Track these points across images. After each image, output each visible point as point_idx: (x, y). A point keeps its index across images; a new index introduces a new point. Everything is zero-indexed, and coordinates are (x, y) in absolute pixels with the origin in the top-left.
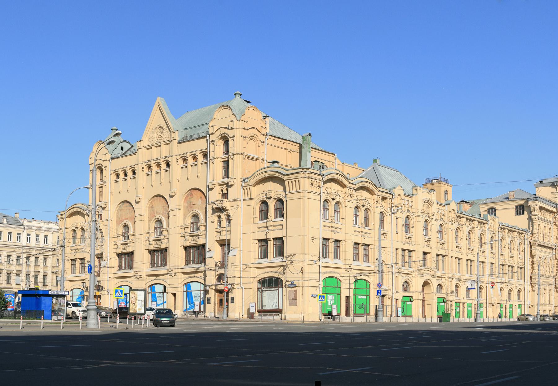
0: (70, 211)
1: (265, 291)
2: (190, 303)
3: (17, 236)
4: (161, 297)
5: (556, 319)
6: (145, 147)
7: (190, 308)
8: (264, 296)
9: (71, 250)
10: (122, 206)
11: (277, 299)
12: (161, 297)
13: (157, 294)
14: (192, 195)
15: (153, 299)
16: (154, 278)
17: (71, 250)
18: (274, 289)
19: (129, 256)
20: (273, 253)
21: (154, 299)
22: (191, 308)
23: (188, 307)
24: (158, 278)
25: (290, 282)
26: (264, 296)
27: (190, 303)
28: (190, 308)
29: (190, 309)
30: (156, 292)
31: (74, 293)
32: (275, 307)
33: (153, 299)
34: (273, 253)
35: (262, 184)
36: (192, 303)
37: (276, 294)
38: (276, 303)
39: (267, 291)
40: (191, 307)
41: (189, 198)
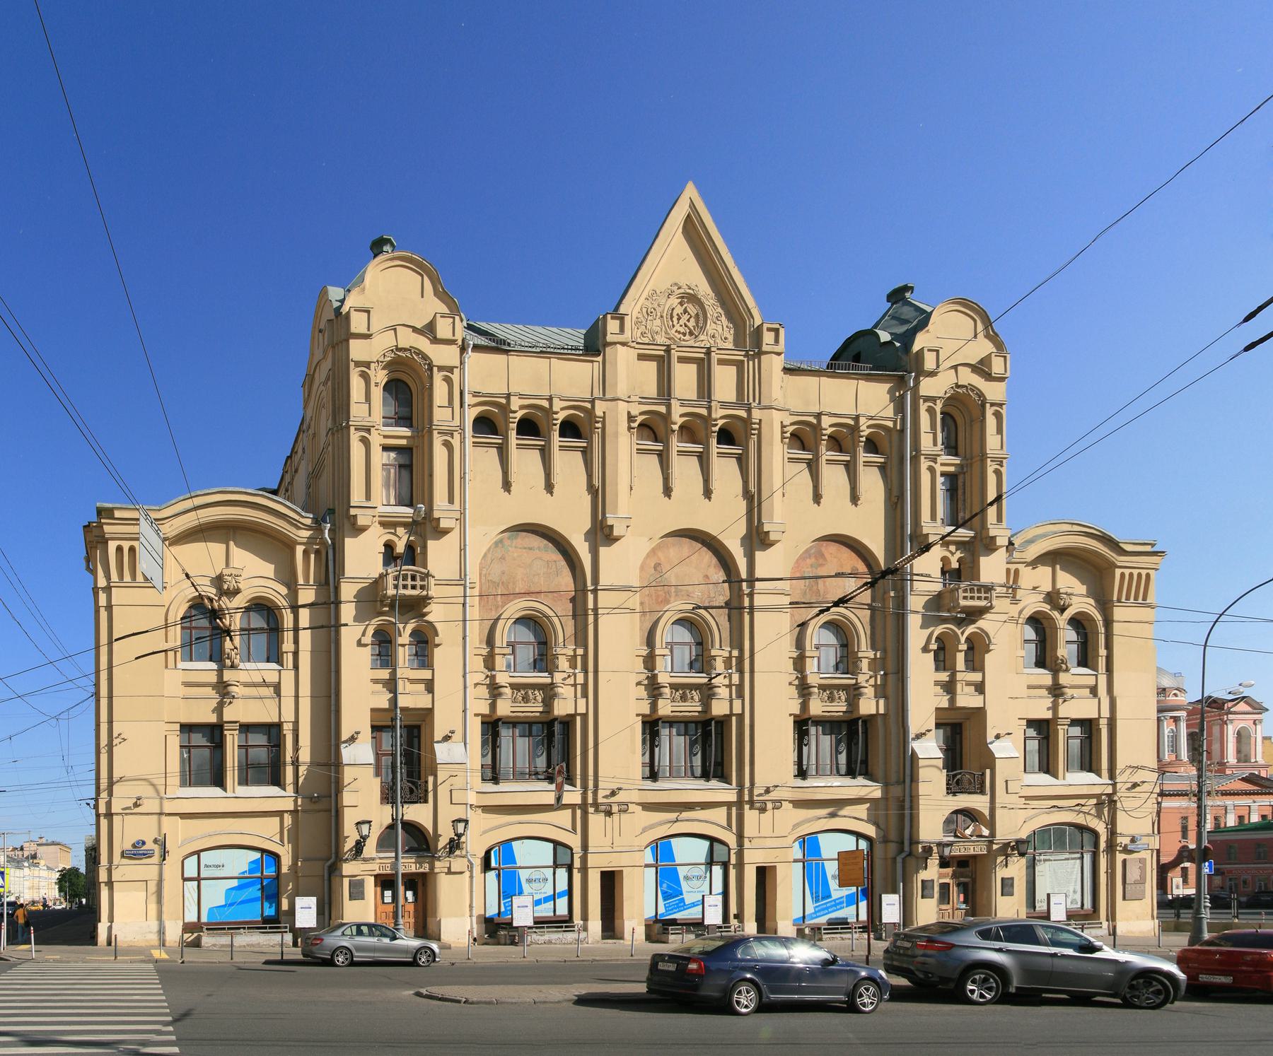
0: (202, 512)
1: (1045, 860)
2: (817, 897)
3: (1154, 715)
4: (699, 878)
5: (930, 973)
6: (637, 346)
7: (819, 911)
8: (1041, 874)
9: (187, 684)
10: (507, 542)
11: (1076, 882)
12: (699, 878)
13: (682, 872)
14: (823, 556)
15: (665, 885)
16: (673, 816)
17: (187, 684)
18: (1067, 856)
19: (530, 735)
20: (110, 697)
21: (669, 887)
22: (822, 913)
23: (810, 909)
24: (685, 815)
25: (1129, 839)
26: (1041, 874)
27: (817, 897)
28: (815, 912)
29: (817, 917)
30: (678, 862)
31: (206, 866)
32: (1072, 903)
33: (665, 885)
34: (110, 697)
35: (1031, 567)
36: (823, 898)
37: (1074, 868)
38: (1075, 892)
39: (1049, 860)
40: (823, 909)
41: (812, 566)
